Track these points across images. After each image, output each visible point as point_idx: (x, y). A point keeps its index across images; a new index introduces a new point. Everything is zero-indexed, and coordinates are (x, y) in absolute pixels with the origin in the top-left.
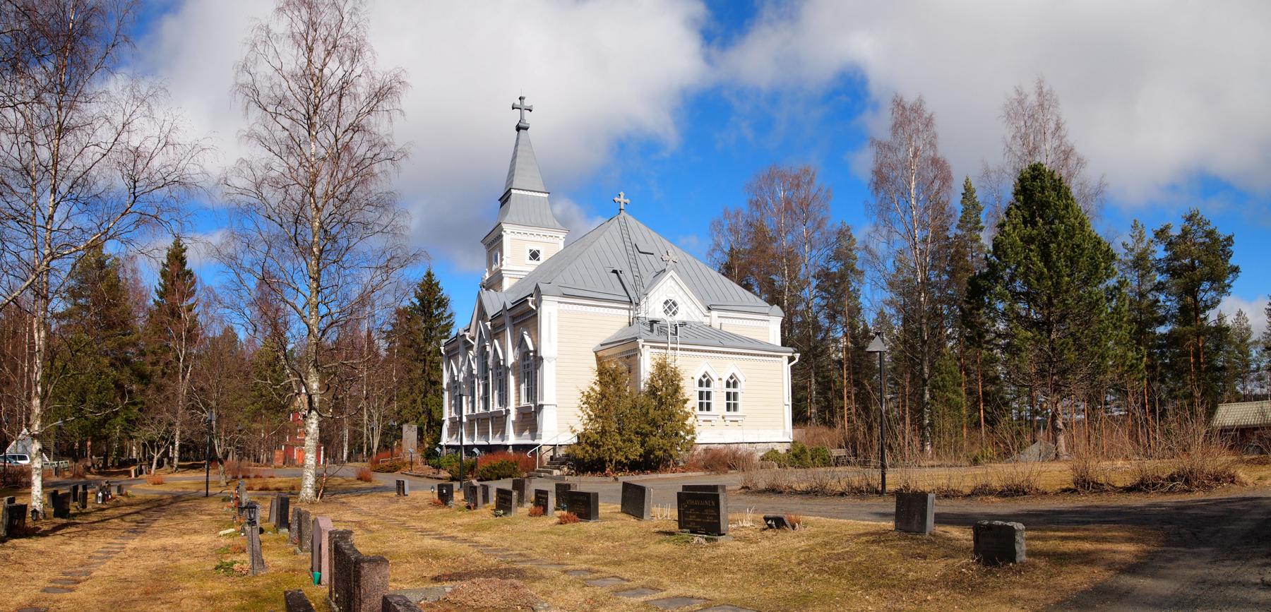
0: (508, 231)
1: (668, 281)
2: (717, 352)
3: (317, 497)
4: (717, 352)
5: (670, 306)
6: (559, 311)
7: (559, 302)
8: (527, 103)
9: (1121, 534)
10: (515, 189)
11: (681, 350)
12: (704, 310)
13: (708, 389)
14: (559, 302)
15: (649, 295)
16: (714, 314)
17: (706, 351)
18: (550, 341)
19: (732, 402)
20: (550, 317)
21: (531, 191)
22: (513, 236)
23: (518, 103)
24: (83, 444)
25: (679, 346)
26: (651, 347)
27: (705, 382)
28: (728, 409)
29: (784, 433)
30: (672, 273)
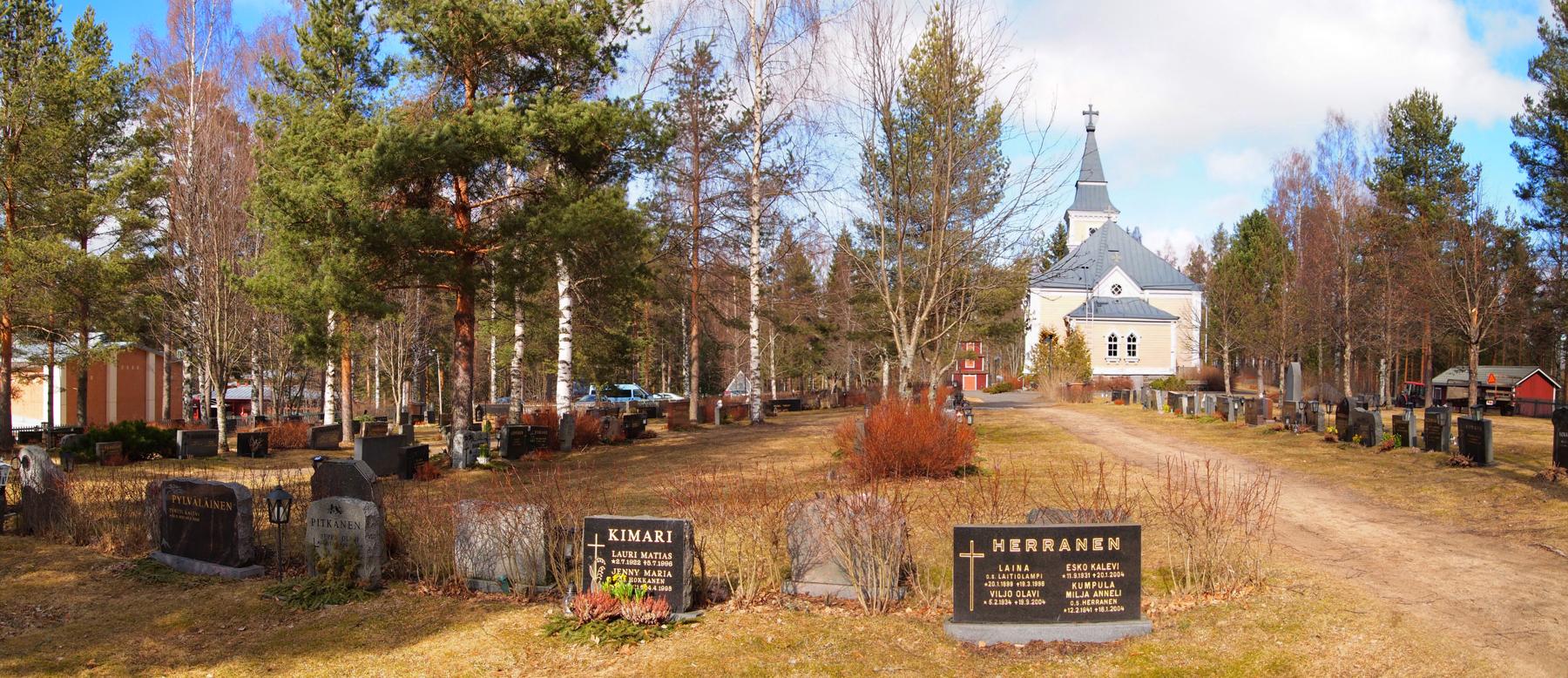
8: (1094, 110)
19: (1132, 350)
23: (1087, 109)
27: (1113, 338)
28: (1110, 354)
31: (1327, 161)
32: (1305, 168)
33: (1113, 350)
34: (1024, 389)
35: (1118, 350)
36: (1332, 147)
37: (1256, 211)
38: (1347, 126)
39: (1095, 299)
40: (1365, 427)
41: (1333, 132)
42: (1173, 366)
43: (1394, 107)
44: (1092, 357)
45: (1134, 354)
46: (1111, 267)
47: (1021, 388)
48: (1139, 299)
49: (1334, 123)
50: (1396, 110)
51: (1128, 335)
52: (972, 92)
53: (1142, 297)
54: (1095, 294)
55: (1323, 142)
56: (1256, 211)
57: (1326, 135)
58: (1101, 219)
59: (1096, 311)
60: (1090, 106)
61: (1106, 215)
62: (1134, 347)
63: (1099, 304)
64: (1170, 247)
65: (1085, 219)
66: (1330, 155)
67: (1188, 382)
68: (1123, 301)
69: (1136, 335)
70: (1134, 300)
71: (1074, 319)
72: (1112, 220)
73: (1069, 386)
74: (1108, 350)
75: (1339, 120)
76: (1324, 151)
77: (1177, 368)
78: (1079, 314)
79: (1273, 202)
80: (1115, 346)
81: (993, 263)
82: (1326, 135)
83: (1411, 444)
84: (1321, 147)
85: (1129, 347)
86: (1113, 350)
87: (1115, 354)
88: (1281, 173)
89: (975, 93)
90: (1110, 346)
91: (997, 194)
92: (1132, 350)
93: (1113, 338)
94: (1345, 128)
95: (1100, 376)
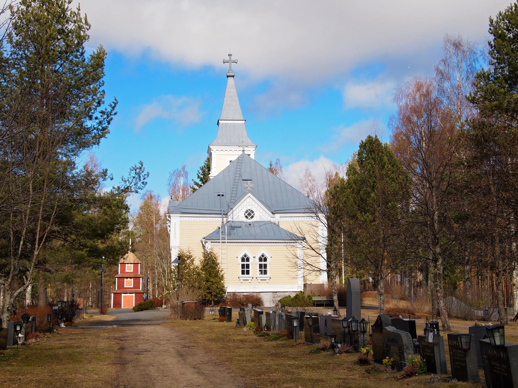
0: (214, 150)
1: (248, 199)
2: (253, 242)
3: (505, 306)
4: (253, 242)
5: (250, 214)
6: (180, 221)
7: (180, 217)
8: (233, 58)
9: (447, 357)
10: (221, 120)
11: (228, 242)
12: (271, 214)
13: (248, 263)
14: (180, 217)
15: (234, 209)
16: (277, 216)
17: (246, 242)
18: (175, 238)
19: (263, 269)
20: (175, 225)
21: (232, 120)
22: (218, 152)
23: (227, 58)
24: (124, 234)
25: (226, 241)
26: (212, 242)
27: (245, 259)
28: (243, 273)
29: (298, 287)
30: (250, 194)
31: (446, 85)
32: (428, 94)
33: (245, 270)
34: (164, 306)
35: (250, 269)
36: (451, 71)
37: (369, 137)
38: (465, 49)
39: (230, 223)
40: (394, 349)
41: (450, 57)
42: (301, 283)
43: (495, 20)
44: (225, 276)
45: (265, 272)
46: (244, 194)
47: (161, 306)
48: (270, 222)
49: (452, 49)
50: (497, 22)
51: (259, 255)
52: (79, 37)
53: (273, 220)
54: (230, 219)
55: (442, 68)
56: (369, 137)
57: (444, 61)
58: (236, 153)
59: (229, 234)
60: (230, 55)
61: (241, 149)
62: (265, 266)
63: (232, 228)
64: (310, 175)
65: (222, 153)
66: (449, 79)
67: (315, 299)
68: (256, 225)
69: (267, 255)
70: (265, 223)
71: (209, 242)
72: (247, 152)
73: (183, 304)
74: (250, 269)
75: (457, 45)
76: (443, 76)
77: (305, 285)
78: (212, 238)
79: (397, 128)
80: (248, 266)
81: (102, 195)
82: (444, 61)
83: (438, 371)
84: (440, 73)
85: (261, 266)
86: (245, 270)
87: (248, 272)
88: (404, 101)
89: (81, 39)
90: (243, 266)
91: (104, 129)
92: (263, 269)
93: (245, 259)
94: (464, 52)
95: (234, 294)
